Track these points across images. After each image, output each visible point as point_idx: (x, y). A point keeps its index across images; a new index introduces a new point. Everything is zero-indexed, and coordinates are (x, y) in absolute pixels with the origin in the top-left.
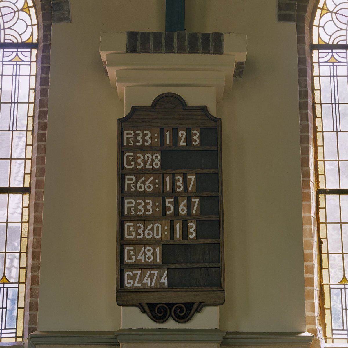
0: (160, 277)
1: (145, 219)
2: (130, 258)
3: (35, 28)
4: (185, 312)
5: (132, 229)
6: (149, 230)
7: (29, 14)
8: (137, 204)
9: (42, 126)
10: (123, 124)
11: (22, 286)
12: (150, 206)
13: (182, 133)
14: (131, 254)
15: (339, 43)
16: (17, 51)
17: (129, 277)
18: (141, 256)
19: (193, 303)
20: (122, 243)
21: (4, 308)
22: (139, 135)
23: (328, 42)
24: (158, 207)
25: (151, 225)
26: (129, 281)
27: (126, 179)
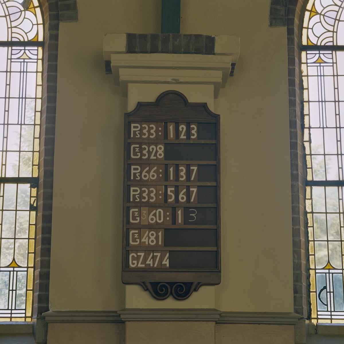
3: (41, 27)
4: (183, 291)
5: (136, 214)
6: (153, 215)
7: (35, 13)
8: (142, 192)
11: (31, 270)
14: (135, 237)
15: (326, 45)
16: (319, 54)
17: (134, 258)
18: (145, 239)
21: (14, 290)
22: (145, 191)
23: (316, 43)
24: (160, 195)
25: (154, 211)
26: (134, 262)
27: (132, 127)
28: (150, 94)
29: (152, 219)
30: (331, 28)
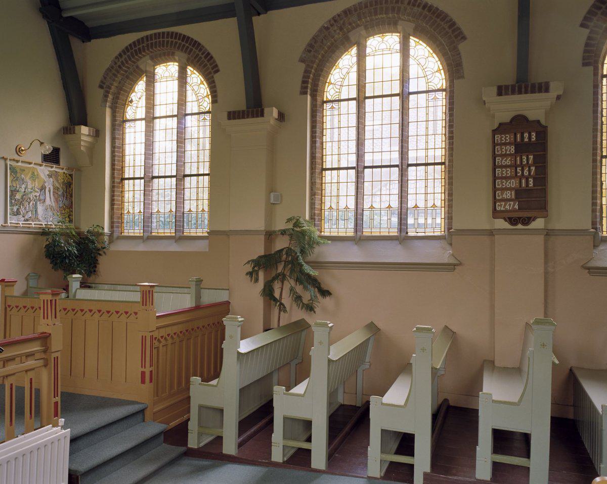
0: (514, 205)
1: (506, 178)
2: (499, 196)
4: (527, 221)
8: (502, 171)
9: (451, 132)
10: (495, 132)
11: (443, 209)
12: (509, 172)
13: (526, 135)
19: (531, 217)
20: (495, 190)
28: (506, 117)
29: (504, 163)
30: (338, 91)
